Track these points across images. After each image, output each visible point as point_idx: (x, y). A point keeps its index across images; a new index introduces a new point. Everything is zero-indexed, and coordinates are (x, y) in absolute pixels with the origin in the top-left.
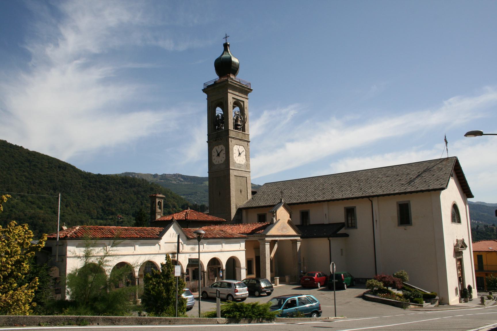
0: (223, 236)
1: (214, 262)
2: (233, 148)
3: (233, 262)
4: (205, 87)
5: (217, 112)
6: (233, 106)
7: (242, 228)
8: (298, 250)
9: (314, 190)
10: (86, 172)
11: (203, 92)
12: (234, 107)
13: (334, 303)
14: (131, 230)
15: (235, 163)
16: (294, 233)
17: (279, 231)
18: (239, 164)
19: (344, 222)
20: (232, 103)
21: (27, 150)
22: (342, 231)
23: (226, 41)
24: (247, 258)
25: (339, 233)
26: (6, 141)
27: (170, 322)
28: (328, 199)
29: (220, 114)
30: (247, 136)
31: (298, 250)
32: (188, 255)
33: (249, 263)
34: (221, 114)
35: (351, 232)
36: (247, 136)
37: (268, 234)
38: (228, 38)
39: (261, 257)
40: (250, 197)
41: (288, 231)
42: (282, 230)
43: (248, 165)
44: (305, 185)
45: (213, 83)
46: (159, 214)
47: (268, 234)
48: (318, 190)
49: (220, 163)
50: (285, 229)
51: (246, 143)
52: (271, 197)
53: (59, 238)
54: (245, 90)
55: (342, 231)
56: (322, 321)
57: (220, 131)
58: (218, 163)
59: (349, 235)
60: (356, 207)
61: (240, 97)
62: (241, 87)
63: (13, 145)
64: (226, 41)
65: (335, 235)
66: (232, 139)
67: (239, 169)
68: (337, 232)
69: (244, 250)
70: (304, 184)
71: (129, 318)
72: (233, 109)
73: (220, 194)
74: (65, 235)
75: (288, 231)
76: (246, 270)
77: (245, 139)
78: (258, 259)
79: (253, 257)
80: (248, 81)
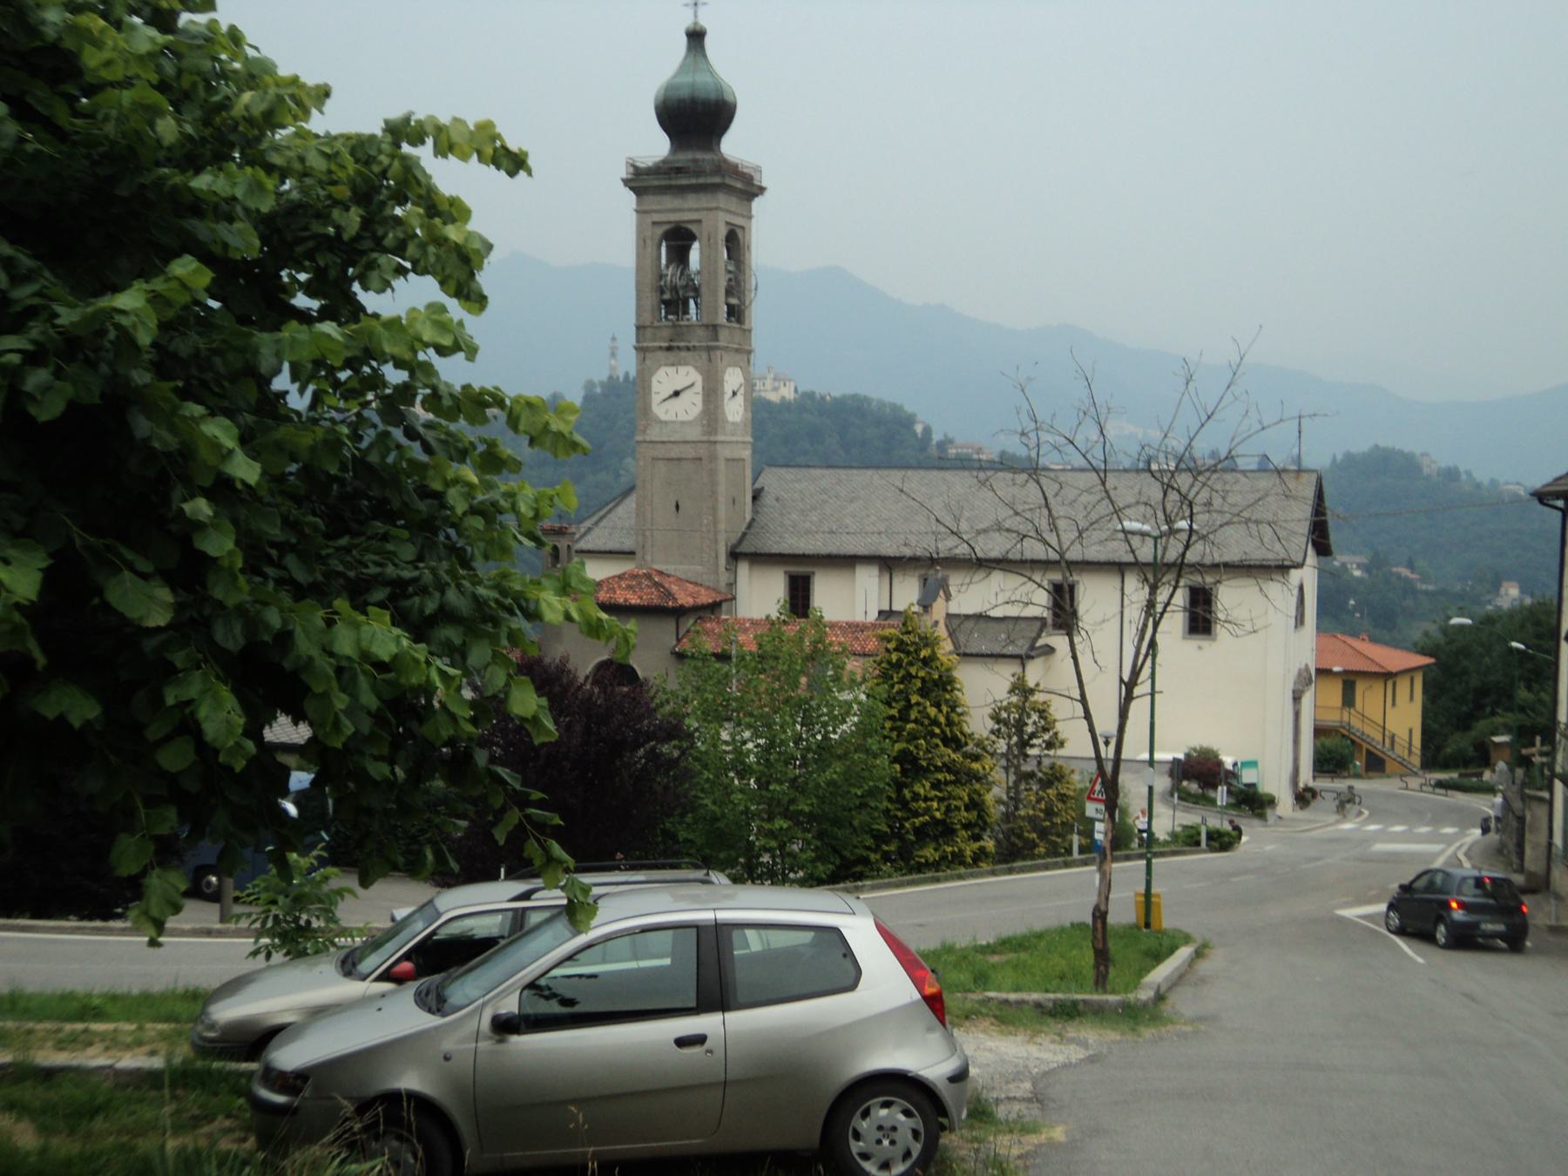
11: (1300, 670)
38: (702, 10)
58: (674, 418)
64: (696, 16)
66: (723, 353)
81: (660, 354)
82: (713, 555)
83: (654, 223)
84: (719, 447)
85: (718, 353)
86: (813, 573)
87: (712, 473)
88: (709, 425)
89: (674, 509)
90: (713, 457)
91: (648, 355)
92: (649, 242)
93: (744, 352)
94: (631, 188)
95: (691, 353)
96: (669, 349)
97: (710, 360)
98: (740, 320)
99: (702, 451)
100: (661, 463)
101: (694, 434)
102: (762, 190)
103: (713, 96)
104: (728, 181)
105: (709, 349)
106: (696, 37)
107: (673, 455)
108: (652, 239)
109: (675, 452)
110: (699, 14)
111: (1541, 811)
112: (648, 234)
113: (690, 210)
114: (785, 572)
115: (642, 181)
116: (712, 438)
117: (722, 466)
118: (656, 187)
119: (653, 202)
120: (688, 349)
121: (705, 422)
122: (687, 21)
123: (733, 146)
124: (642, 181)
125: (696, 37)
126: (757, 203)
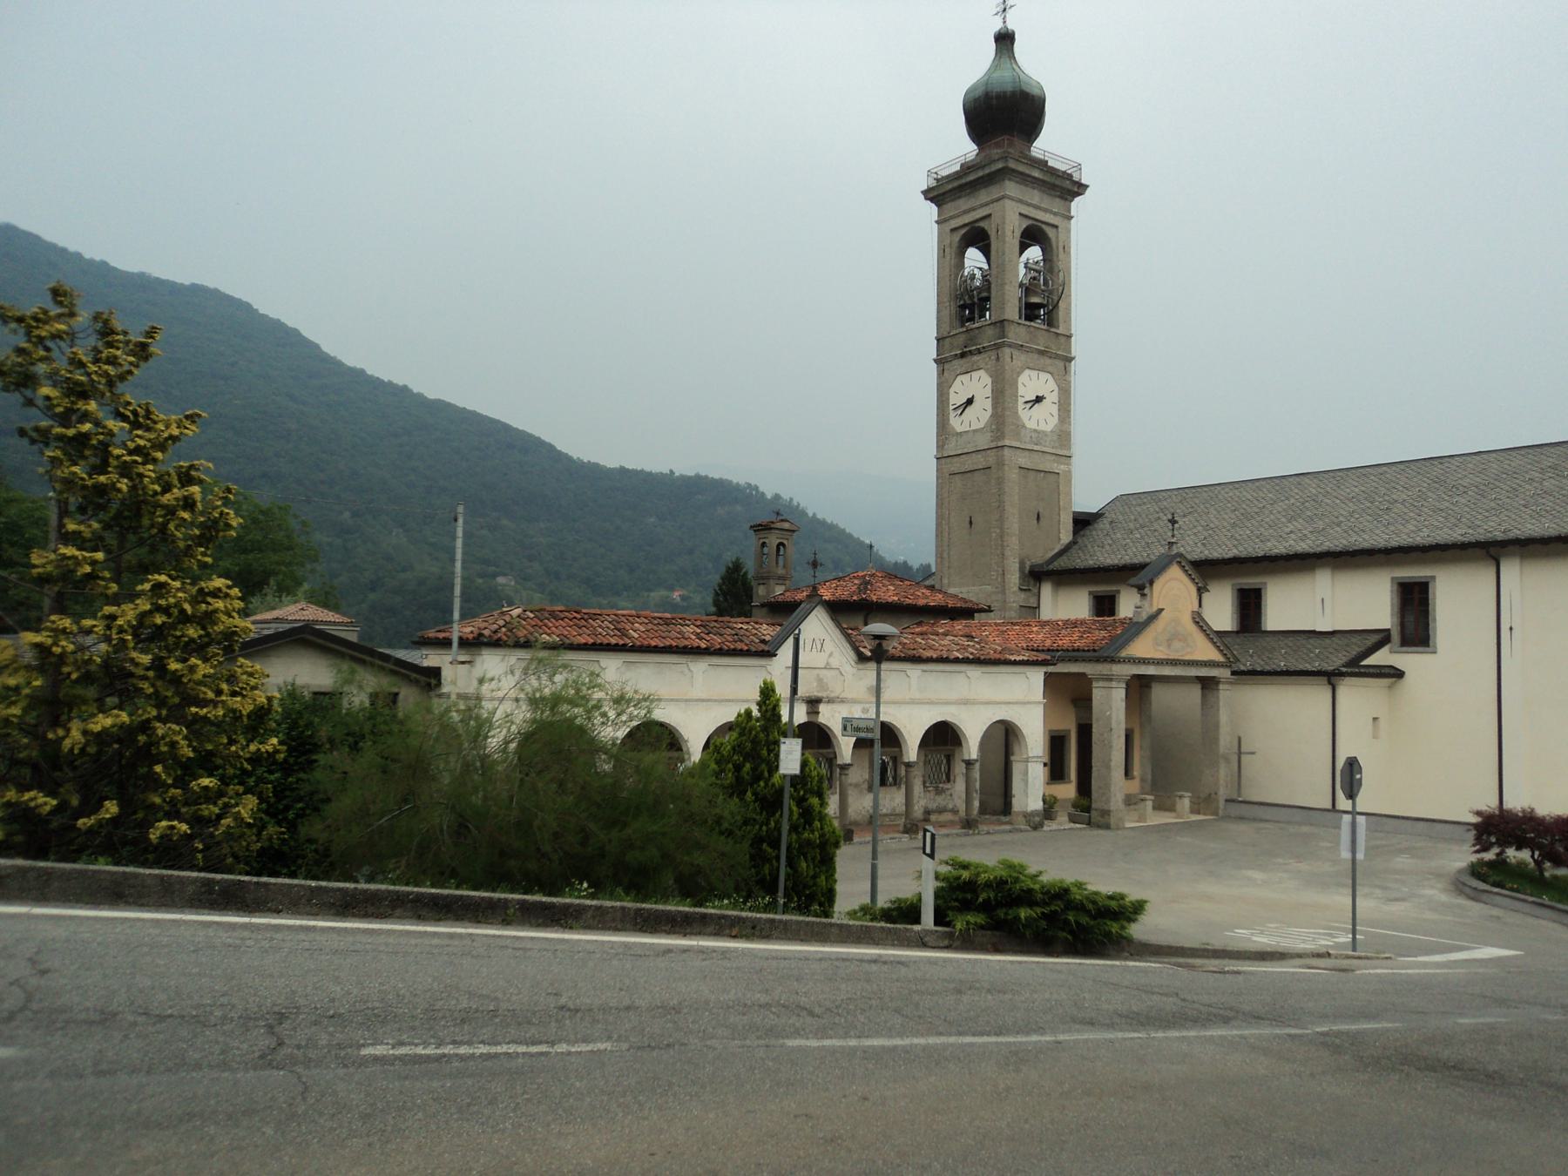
0: (972, 654)
1: (943, 737)
2: (1017, 382)
3: (1005, 736)
4: (933, 183)
5: (967, 263)
6: (1021, 242)
7: (1038, 633)
8: (1518, 953)
9: (1283, 520)
10: (386, 380)
11: (926, 199)
12: (1023, 247)
13: (1351, 915)
14: (680, 624)
15: (1024, 426)
16: (1214, 655)
17: (1161, 648)
18: (1035, 431)
19: (1388, 627)
20: (1018, 234)
21: (420, 396)
22: (1380, 658)
23: (1005, 22)
24: (1050, 731)
25: (1365, 663)
26: (362, 372)
27: (754, 928)
28: (1333, 548)
29: (976, 271)
30: (1062, 339)
31: (1518, 953)
32: (859, 710)
33: (1056, 743)
34: (980, 269)
35: (1408, 660)
36: (1062, 339)
37: (1124, 654)
38: (1010, 14)
39: (1094, 726)
40: (1066, 536)
41: (1189, 650)
42: (1169, 642)
43: (1063, 435)
44: (1255, 502)
45: (957, 168)
46: (781, 582)
47: (1124, 654)
48: (1300, 520)
49: (973, 428)
50: (1180, 640)
51: (1060, 364)
52: (1137, 538)
53: (461, 638)
54: (1066, 187)
55: (1380, 658)
56: (1300, 967)
57: (977, 325)
58: (968, 429)
59: (1404, 673)
60: (1437, 580)
61: (1041, 207)
62: (1371, 971)
63: (411, 391)
64: (1005, 22)
65: (1355, 668)
66: (1016, 353)
67: (1036, 448)
68: (1363, 660)
69: (1039, 703)
70: (1250, 497)
71: (612, 907)
72: (1021, 252)
73: (971, 523)
74: (476, 631)
75: (1189, 650)
76: (1045, 765)
77: (1059, 349)
78: (1085, 732)
79: (1069, 725)
80: (1076, 157)
81: (956, 362)
82: (1001, 572)
83: (953, 230)
84: (1006, 451)
85: (1007, 351)
86: (1118, 592)
87: (1000, 482)
88: (998, 430)
89: (968, 525)
90: (1001, 464)
91: (946, 366)
92: (947, 250)
93: (1059, 358)
94: (932, 200)
95: (983, 356)
96: (963, 355)
97: (998, 359)
98: (1051, 321)
99: (991, 458)
100: (957, 477)
101: (983, 441)
102: (1087, 186)
103: (1009, 88)
104: (1012, 164)
105: (998, 347)
106: (1005, 40)
107: (968, 467)
108: (951, 247)
109: (969, 463)
110: (1008, 20)
111: (1136, 818)
112: (947, 242)
113: (982, 206)
114: (1090, 593)
115: (942, 193)
116: (1000, 444)
117: (1013, 475)
118: (950, 191)
119: (952, 208)
120: (979, 352)
121: (993, 427)
122: (997, 26)
123: (1051, 144)
124: (942, 193)
125: (1005, 40)
126: (1077, 205)
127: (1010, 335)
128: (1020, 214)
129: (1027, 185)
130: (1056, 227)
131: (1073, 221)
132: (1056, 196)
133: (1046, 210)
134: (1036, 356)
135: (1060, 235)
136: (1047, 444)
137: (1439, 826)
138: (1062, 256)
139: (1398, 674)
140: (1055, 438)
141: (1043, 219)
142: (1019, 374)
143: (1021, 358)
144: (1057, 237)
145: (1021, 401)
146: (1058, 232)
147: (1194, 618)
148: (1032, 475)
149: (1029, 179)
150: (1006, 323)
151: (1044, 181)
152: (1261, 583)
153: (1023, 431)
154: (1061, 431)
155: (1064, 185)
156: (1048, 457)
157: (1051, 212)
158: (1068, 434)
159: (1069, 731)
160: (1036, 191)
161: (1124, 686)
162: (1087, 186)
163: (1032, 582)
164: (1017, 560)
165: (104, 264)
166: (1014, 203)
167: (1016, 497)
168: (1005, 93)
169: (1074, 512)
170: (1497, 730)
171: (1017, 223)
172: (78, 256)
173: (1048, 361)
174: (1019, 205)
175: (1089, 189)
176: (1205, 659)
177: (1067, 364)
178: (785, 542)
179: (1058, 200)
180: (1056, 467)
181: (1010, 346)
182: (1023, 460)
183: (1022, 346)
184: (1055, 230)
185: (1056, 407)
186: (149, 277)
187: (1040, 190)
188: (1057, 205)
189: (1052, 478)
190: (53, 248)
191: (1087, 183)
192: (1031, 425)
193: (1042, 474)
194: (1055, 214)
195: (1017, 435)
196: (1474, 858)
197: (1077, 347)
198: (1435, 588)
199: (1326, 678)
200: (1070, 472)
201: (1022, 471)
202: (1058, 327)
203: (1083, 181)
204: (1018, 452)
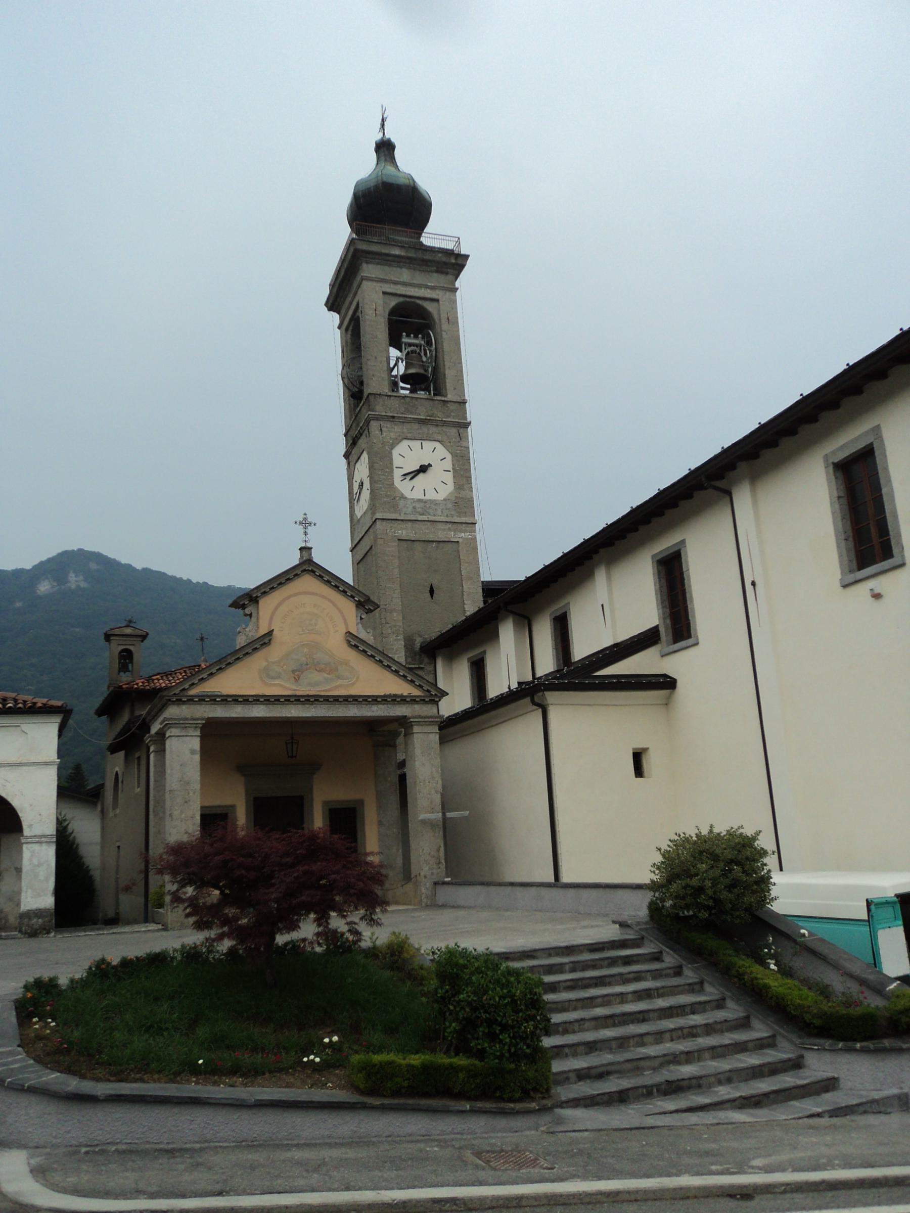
18: (419, 501)
42: (297, 675)
51: (453, 431)
66: (386, 425)
67: (420, 518)
98: (439, 391)
106: (385, 148)
125: (385, 148)
127: (378, 408)
128: (384, 293)
129: (390, 266)
130: (437, 301)
131: (458, 293)
132: (432, 272)
133: (420, 286)
134: (416, 426)
135: (442, 308)
136: (439, 513)
137: (585, 893)
138: (445, 326)
139: (667, 683)
140: (450, 506)
141: (417, 295)
142: (393, 446)
143: (391, 431)
144: (439, 311)
145: (397, 474)
146: (439, 305)
147: (349, 642)
148: (418, 547)
149: (390, 258)
150: (372, 398)
151: (410, 258)
152: (564, 606)
153: (401, 503)
154: (456, 497)
155: (437, 259)
156: (440, 526)
157: (427, 287)
158: (470, 501)
159: (233, 807)
160: (404, 270)
161: (198, 733)
162: (467, 257)
163: (426, 660)
164: (401, 637)
165: (205, 584)
166: (375, 284)
167: (396, 571)
168: (369, 189)
169: (483, 582)
170: (761, 737)
171: (380, 302)
172: (189, 581)
173: (433, 429)
174: (382, 285)
175: (470, 258)
176: (381, 693)
177: (461, 430)
178: (131, 648)
179: (435, 275)
180: (461, 536)
181: (378, 418)
182: (404, 532)
183: (393, 417)
184: (435, 304)
185: (450, 474)
186: (234, 588)
187: (409, 268)
188: (435, 279)
189: (448, 547)
190: (174, 578)
191: (466, 253)
192: (409, 494)
193: (434, 545)
194: (433, 288)
195: (395, 508)
196: (317, 931)
197: (472, 412)
198: (686, 553)
199: (528, 700)
200: (474, 539)
201: (404, 544)
202: (446, 396)
203: (462, 252)
204: (396, 524)
